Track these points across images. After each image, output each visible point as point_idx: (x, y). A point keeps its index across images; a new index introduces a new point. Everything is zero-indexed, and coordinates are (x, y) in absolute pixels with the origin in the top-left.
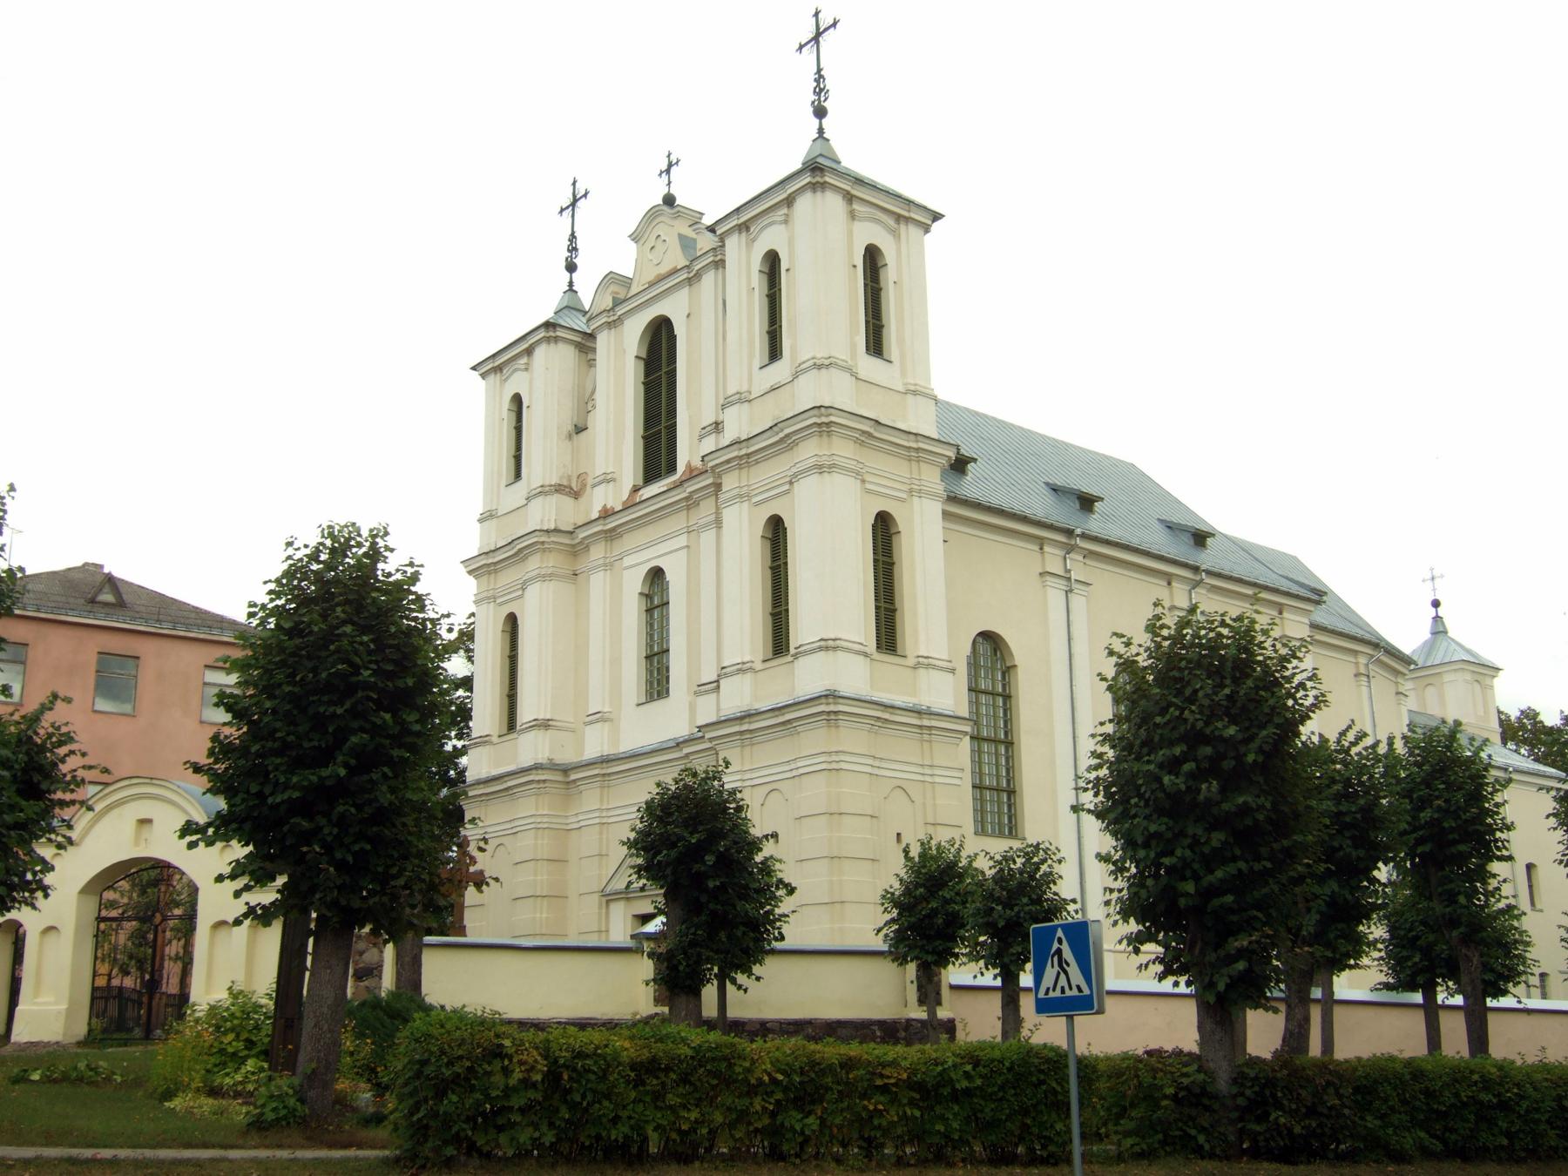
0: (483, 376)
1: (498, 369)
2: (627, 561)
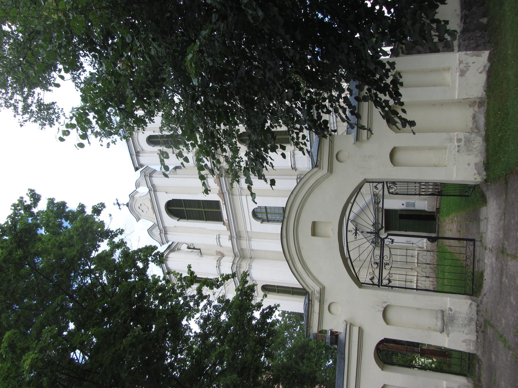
2: (249, 229)
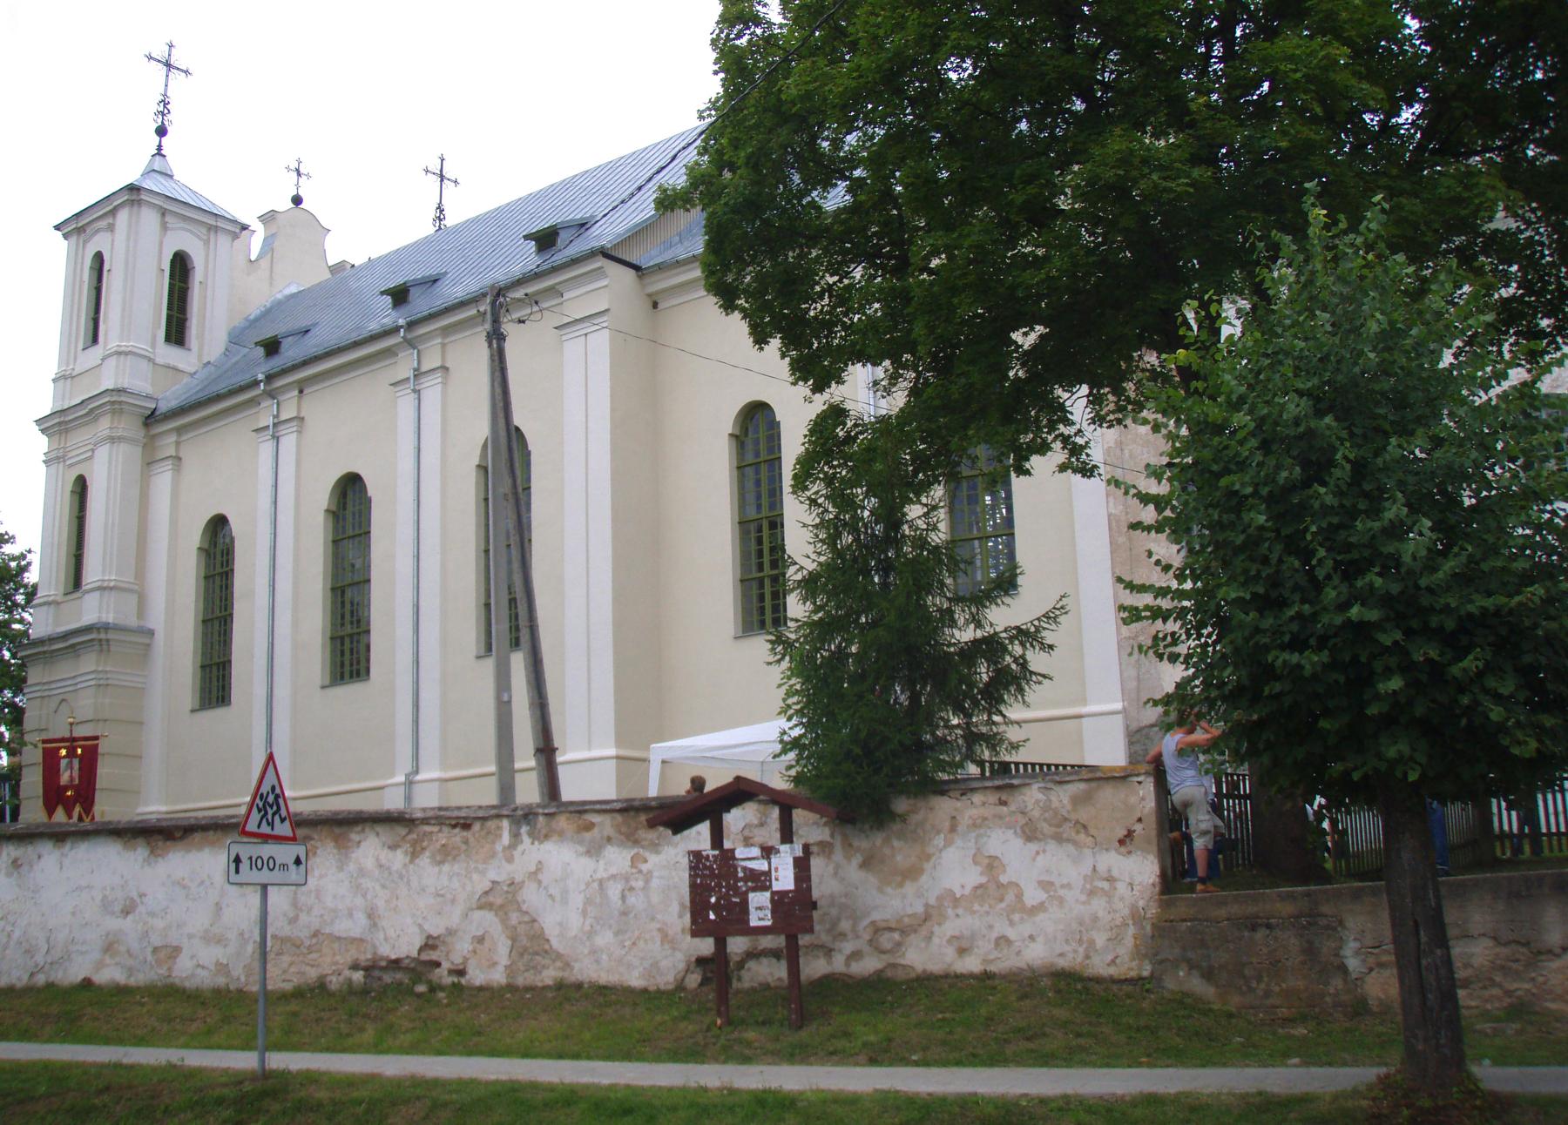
0: (66, 236)
1: (80, 230)
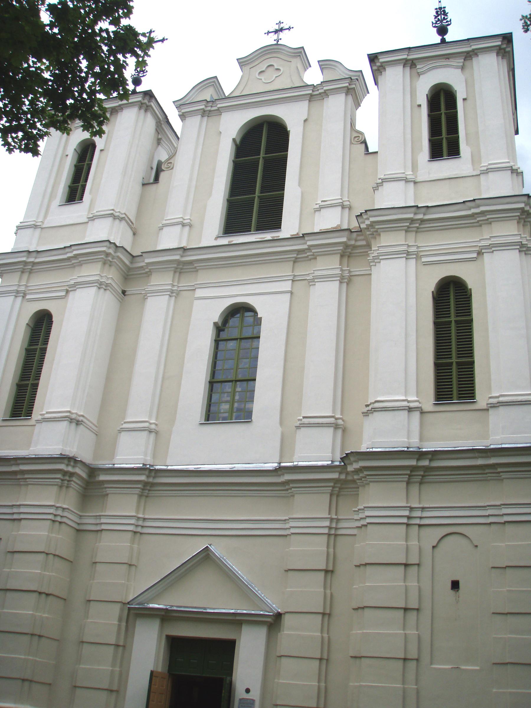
2: (199, 293)
